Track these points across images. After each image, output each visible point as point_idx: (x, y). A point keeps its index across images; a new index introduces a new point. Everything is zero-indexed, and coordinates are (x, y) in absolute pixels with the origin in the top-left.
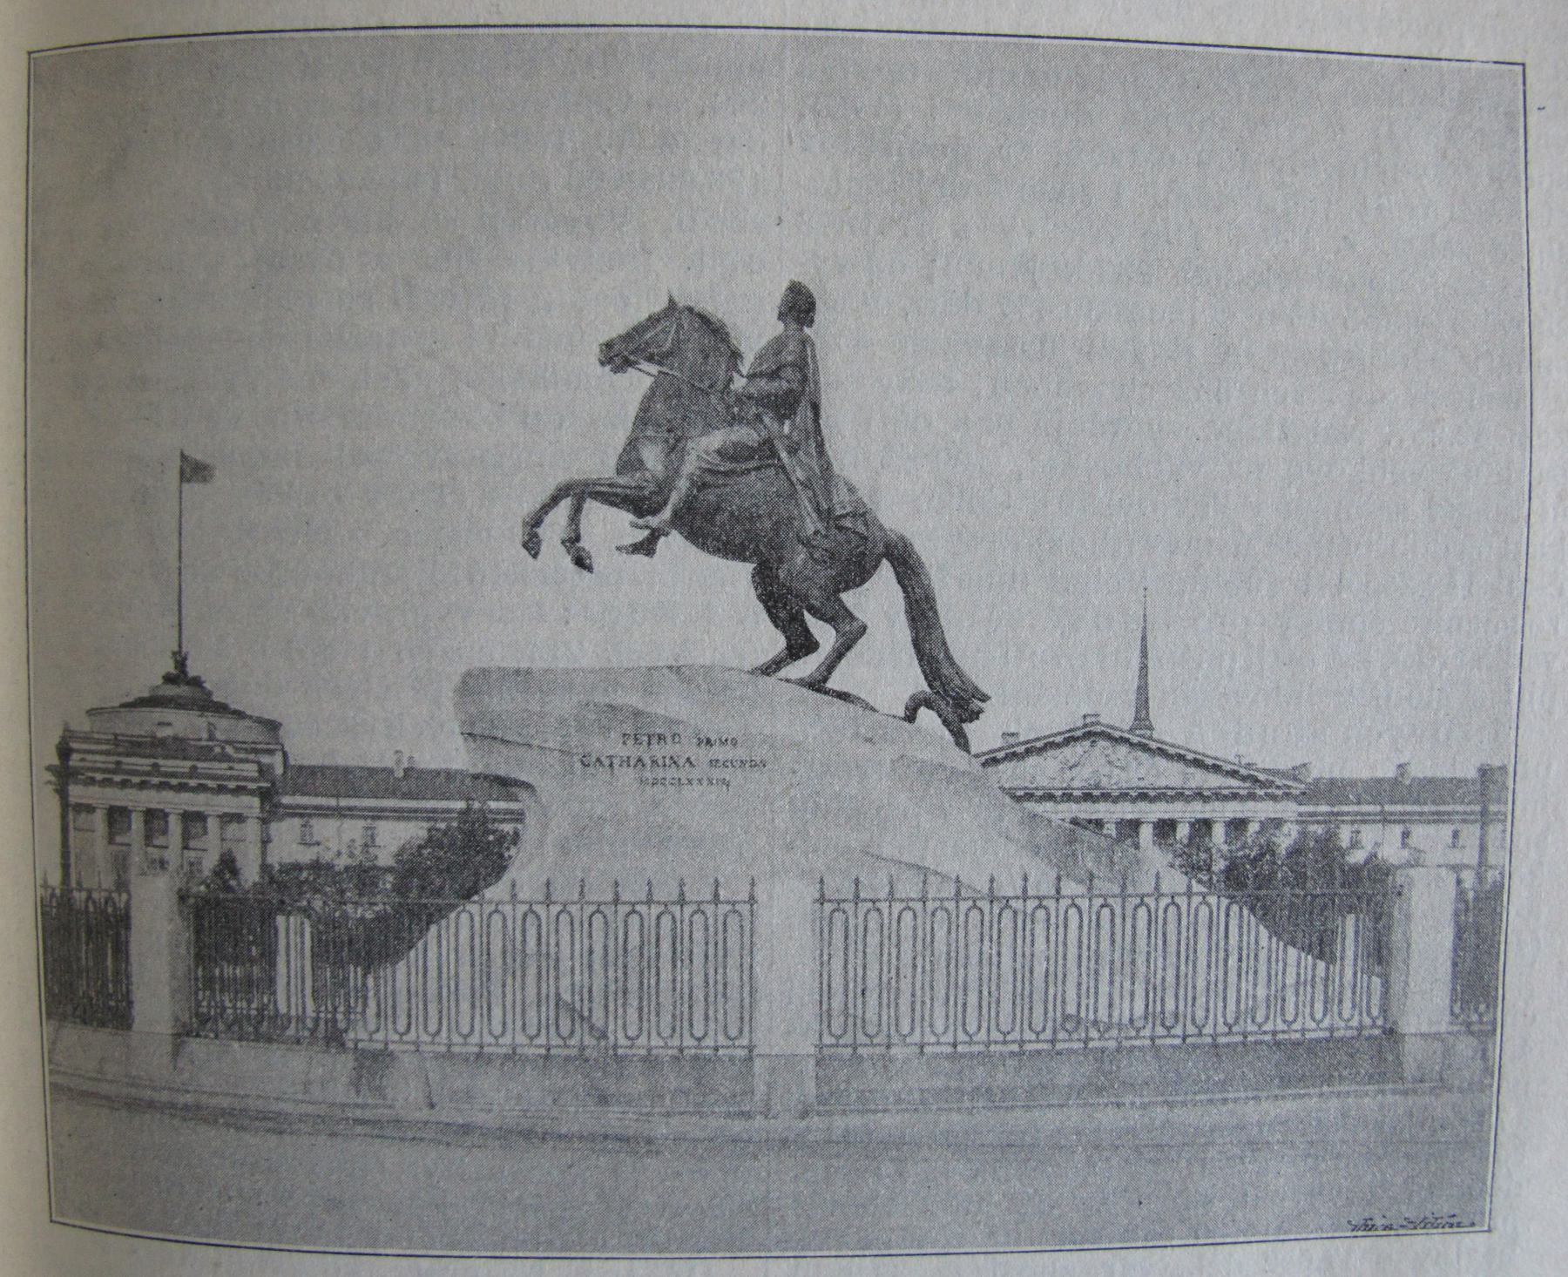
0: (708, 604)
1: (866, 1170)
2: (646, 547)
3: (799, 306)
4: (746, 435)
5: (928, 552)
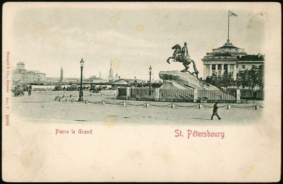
0: (180, 66)
3: (185, 44)
5: (195, 61)
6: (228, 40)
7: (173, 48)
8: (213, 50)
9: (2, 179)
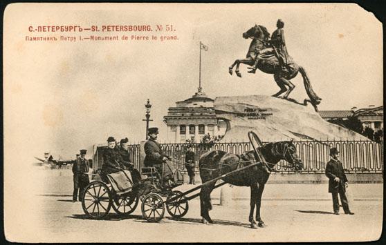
0: (266, 82)
1: (359, 169)
2: (254, 72)
3: (280, 24)
4: (270, 50)
5: (307, 70)
6: (200, 89)
7: (246, 36)
8: (178, 103)
9: (9, 3)
